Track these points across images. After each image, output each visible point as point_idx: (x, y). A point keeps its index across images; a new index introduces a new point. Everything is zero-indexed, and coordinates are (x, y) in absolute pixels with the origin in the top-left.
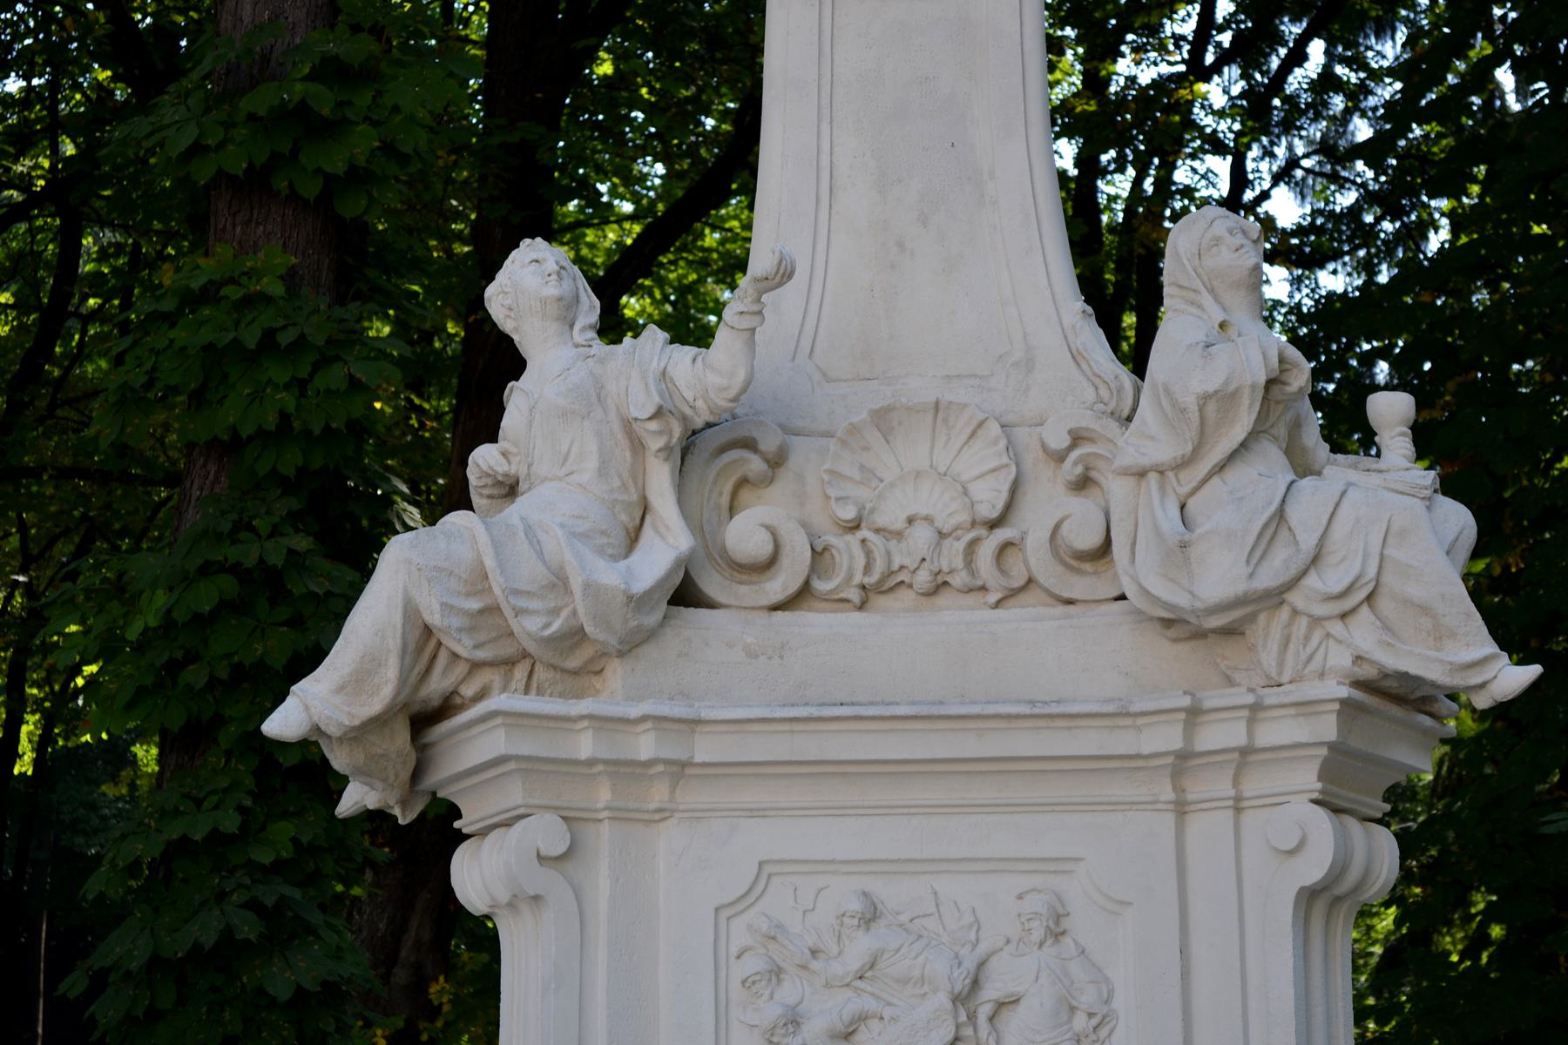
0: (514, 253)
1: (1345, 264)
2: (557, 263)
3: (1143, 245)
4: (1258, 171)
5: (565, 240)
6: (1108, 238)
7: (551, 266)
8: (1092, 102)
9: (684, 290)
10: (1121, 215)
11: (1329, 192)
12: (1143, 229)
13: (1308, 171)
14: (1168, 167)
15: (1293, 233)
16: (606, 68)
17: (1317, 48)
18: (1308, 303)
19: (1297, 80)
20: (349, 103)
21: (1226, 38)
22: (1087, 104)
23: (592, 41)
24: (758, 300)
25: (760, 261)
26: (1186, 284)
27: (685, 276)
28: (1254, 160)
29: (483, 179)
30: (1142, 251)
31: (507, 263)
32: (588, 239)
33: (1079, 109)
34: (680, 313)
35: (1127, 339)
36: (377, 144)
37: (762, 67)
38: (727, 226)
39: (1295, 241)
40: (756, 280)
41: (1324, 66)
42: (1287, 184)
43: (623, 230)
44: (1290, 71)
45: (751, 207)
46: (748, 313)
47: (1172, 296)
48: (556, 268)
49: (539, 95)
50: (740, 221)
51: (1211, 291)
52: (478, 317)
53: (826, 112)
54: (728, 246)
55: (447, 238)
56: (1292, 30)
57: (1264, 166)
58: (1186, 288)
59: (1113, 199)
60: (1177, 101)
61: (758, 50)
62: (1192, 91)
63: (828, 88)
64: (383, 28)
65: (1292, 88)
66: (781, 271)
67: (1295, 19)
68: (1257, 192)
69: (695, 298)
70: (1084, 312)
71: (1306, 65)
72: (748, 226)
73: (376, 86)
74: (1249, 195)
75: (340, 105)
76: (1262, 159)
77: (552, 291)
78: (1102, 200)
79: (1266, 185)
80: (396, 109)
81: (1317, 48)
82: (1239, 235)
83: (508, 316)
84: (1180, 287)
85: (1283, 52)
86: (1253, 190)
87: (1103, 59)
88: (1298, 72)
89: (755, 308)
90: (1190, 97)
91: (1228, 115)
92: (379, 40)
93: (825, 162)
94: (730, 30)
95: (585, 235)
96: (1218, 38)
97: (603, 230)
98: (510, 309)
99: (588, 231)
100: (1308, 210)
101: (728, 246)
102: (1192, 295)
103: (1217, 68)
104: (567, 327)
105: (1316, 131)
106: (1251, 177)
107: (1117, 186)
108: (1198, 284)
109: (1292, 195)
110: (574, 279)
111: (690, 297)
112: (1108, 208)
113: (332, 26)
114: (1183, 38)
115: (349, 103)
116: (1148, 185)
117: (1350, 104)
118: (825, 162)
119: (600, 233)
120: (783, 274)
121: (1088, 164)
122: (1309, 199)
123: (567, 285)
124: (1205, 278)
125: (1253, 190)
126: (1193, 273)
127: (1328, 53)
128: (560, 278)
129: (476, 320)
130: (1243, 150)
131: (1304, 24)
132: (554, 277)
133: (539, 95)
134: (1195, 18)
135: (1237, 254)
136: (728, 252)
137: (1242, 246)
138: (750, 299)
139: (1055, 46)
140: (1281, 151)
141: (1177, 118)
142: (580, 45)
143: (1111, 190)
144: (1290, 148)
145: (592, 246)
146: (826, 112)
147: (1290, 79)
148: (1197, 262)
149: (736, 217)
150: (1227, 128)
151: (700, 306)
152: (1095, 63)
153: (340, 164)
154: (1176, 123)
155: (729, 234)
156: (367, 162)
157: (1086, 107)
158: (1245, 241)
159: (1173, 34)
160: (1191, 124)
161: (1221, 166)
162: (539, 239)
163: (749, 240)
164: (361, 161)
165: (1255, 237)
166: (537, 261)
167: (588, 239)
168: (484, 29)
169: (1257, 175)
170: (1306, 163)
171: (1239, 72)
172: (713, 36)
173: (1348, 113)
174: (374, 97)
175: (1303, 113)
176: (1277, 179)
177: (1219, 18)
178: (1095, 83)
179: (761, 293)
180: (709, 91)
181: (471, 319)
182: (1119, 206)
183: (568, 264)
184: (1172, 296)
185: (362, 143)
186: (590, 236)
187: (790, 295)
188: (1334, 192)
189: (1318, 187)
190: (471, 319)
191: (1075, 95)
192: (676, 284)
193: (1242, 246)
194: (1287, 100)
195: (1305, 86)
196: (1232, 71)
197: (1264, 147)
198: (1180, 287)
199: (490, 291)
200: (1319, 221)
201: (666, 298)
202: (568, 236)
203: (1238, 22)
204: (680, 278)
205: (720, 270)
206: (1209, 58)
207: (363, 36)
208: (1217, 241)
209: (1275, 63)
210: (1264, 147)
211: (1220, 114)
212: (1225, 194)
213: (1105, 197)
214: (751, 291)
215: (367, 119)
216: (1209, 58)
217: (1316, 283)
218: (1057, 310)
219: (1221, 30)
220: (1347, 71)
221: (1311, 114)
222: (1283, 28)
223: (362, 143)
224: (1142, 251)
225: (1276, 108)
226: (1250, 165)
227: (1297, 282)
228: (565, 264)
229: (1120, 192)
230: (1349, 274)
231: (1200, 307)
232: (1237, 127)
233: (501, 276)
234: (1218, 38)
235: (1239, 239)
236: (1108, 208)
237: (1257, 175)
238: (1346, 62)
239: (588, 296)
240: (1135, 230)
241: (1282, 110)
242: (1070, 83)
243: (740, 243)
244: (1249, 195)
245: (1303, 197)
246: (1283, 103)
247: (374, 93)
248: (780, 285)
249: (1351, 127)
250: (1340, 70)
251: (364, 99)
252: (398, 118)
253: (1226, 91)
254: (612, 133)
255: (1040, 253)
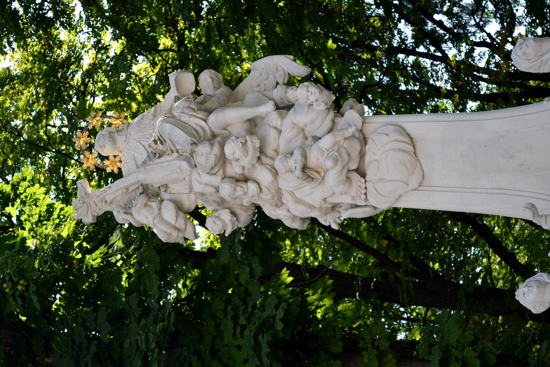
0: (521, 302)
1: (514, 7)
2: (525, 287)
3: (506, 78)
4: (480, 38)
5: (496, 283)
6: (501, 90)
7: (526, 289)
8: (456, 96)
9: (516, 241)
10: (494, 86)
11: (488, 12)
12: (501, 79)
13: (481, 20)
14: (479, 70)
15: (503, 25)
16: (437, 266)
17: (437, 17)
18: (528, 20)
19: (448, 23)
20: (456, 357)
21: (432, 49)
22: (456, 98)
23: (430, 271)
24: (541, 216)
25: (528, 216)
26: (539, 65)
27: (510, 241)
28: (476, 39)
29: (478, 311)
30: (508, 79)
31: (524, 305)
32: (496, 275)
33: (458, 101)
34: (524, 243)
35: (539, 84)
36: (470, 348)
37: (440, 211)
38: (493, 225)
39: (505, 24)
40: (534, 217)
41: (444, 14)
42: (485, 27)
43: (493, 262)
44: (445, 26)
45: (487, 216)
46: (546, 220)
47: (543, 70)
48: (526, 288)
49: (449, 290)
50: (491, 221)
51: (542, 56)
52: (528, 316)
53: (472, 190)
54: (500, 225)
55: (497, 325)
56: (430, 26)
57: (478, 35)
58: (541, 64)
59: (488, 88)
60: (456, 66)
61: (434, 212)
62: (453, 61)
63: (464, 189)
64: (430, 344)
65: (451, 26)
66: (531, 208)
67: (426, 24)
68: (487, 38)
69: (519, 237)
70: (547, 101)
71: (443, 21)
72: (493, 217)
73: (450, 347)
74: (488, 40)
75: (457, 360)
76: (476, 36)
77: (535, 289)
78: (488, 92)
79: (485, 34)
80: (458, 341)
81: (437, 17)
82: (522, 46)
83: (544, 305)
84: (540, 67)
85: (438, 29)
86: (486, 39)
87: (441, 92)
88: (445, 23)
89: (544, 217)
90: (455, 62)
91: (460, 48)
92: (434, 345)
93: (491, 191)
94: (426, 222)
95: (495, 276)
96: (432, 51)
97: (493, 269)
98: (541, 305)
99: (493, 275)
100: (494, 20)
101: (500, 225)
102: (543, 63)
103: (443, 52)
104: (548, 285)
105: (466, 17)
106: (482, 40)
107: (484, 88)
108: (539, 61)
109: (488, 26)
110: (531, 281)
111: (519, 240)
112: (491, 90)
113: (429, 361)
114: (432, 64)
115: (456, 357)
116: (485, 76)
117: (457, 6)
118: (491, 191)
119: (494, 271)
120: (532, 207)
121: (477, 97)
122: (490, 19)
123: (533, 284)
124: (537, 58)
125: (486, 39)
126: (535, 62)
127: (438, 13)
128: (530, 286)
129: (529, 317)
130: (473, 43)
131: (428, 21)
132: (530, 288)
133: (449, 290)
134: (425, 59)
135: (529, 47)
136: (503, 225)
137: (526, 45)
138: (541, 220)
139: (435, 110)
140: (473, 29)
141: (462, 66)
142: (432, 275)
143: (484, 89)
144: (471, 26)
145: (499, 274)
146: (472, 190)
147: (448, 26)
148: (532, 61)
149: (490, 222)
150: (464, 48)
151: (522, 235)
152: (442, 95)
153: (477, 362)
154: (464, 66)
155: (496, 224)
156: (477, 352)
157: (457, 98)
158: (525, 44)
159: (431, 67)
160: (462, 61)
161: (478, 50)
162: (516, 293)
163: (498, 216)
164: (476, 354)
165: (523, 40)
166: (524, 294)
167: (496, 275)
168: (420, 308)
169: (481, 38)
170: (478, 20)
171: (444, 44)
172: (430, 228)
173: (460, 6)
174: (454, 348)
175: (460, 22)
176: (483, 30)
177: (425, 51)
178: (449, 95)
179: (539, 215)
180: (447, 230)
181: (528, 318)
182: (490, 86)
183: (525, 283)
184: (543, 70)
185: (470, 353)
186: (495, 274)
187: (539, 205)
188: (488, 10)
189: (486, 16)
190: (528, 318)
191: (453, 101)
192: (513, 244)
193: (526, 45)
194: (455, 27)
195: (450, 21)
196: (444, 46)
197: (471, 35)
198: (540, 67)
199: (534, 311)
200: (498, 16)
201: (518, 248)
202: (495, 282)
203: (427, 44)
204: (511, 243)
205: (509, 228)
206: (439, 54)
207: (433, 350)
208: (524, 54)
209: (441, 32)
210: (471, 35)
211: (460, 51)
212: (488, 49)
213: (487, 91)
214: (538, 219)
215: (462, 351)
216: (439, 54)
217: (521, 17)
218: (547, 110)
219: (429, 50)
220: (445, 6)
221: (460, 19)
222: (429, 29)
223: (470, 353)
224: (508, 79)
225: (457, 31)
226: (478, 40)
227: (520, 23)
228: (525, 285)
229: (485, 86)
230: (518, 5)
231: (548, 60)
232: (464, 44)
233: (529, 307)
234: (432, 51)
235: (524, 46)
236: (491, 90)
237: (481, 38)
238: (442, 7)
239: (537, 277)
240: (501, 81)
241: (458, 30)
242: (447, 104)
243: (500, 221)
244: (488, 40)
245: (489, 21)
246: (456, 29)
247: (453, 349)
248: (536, 208)
249: (464, 5)
250: (445, 9)
251: (455, 352)
252: (462, 340)
253: (450, 48)
254: (460, 266)
255: (526, 116)
